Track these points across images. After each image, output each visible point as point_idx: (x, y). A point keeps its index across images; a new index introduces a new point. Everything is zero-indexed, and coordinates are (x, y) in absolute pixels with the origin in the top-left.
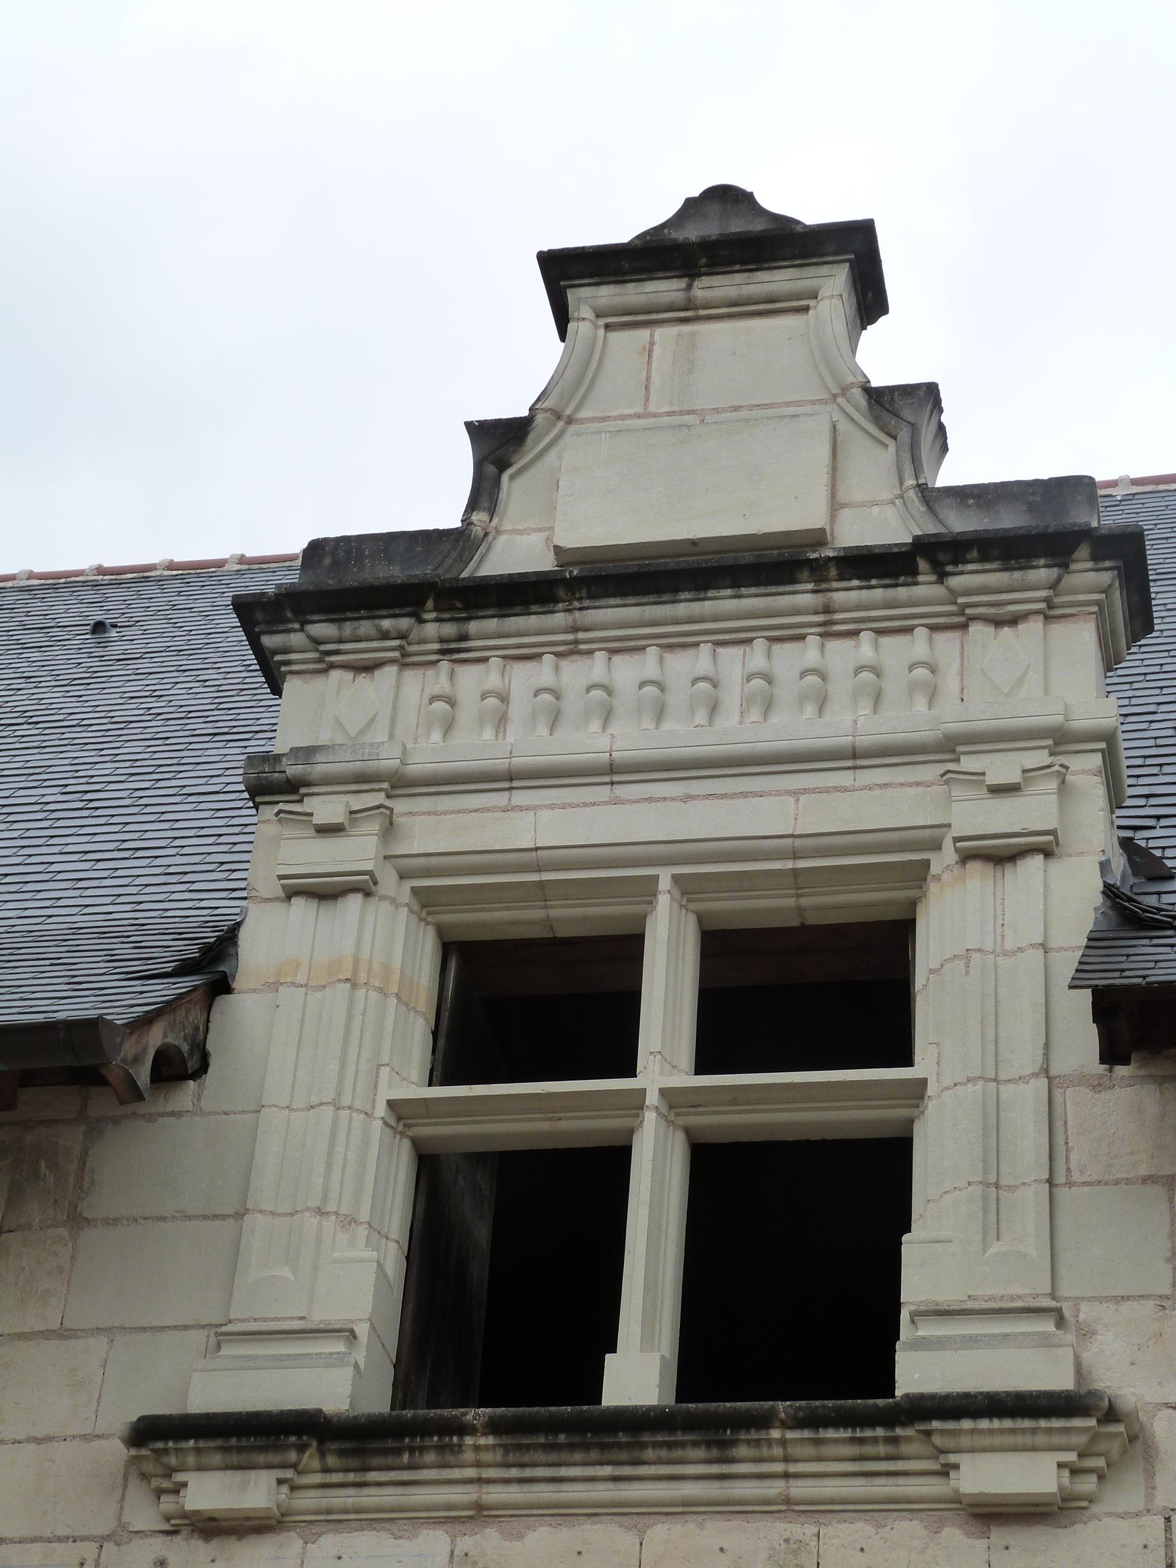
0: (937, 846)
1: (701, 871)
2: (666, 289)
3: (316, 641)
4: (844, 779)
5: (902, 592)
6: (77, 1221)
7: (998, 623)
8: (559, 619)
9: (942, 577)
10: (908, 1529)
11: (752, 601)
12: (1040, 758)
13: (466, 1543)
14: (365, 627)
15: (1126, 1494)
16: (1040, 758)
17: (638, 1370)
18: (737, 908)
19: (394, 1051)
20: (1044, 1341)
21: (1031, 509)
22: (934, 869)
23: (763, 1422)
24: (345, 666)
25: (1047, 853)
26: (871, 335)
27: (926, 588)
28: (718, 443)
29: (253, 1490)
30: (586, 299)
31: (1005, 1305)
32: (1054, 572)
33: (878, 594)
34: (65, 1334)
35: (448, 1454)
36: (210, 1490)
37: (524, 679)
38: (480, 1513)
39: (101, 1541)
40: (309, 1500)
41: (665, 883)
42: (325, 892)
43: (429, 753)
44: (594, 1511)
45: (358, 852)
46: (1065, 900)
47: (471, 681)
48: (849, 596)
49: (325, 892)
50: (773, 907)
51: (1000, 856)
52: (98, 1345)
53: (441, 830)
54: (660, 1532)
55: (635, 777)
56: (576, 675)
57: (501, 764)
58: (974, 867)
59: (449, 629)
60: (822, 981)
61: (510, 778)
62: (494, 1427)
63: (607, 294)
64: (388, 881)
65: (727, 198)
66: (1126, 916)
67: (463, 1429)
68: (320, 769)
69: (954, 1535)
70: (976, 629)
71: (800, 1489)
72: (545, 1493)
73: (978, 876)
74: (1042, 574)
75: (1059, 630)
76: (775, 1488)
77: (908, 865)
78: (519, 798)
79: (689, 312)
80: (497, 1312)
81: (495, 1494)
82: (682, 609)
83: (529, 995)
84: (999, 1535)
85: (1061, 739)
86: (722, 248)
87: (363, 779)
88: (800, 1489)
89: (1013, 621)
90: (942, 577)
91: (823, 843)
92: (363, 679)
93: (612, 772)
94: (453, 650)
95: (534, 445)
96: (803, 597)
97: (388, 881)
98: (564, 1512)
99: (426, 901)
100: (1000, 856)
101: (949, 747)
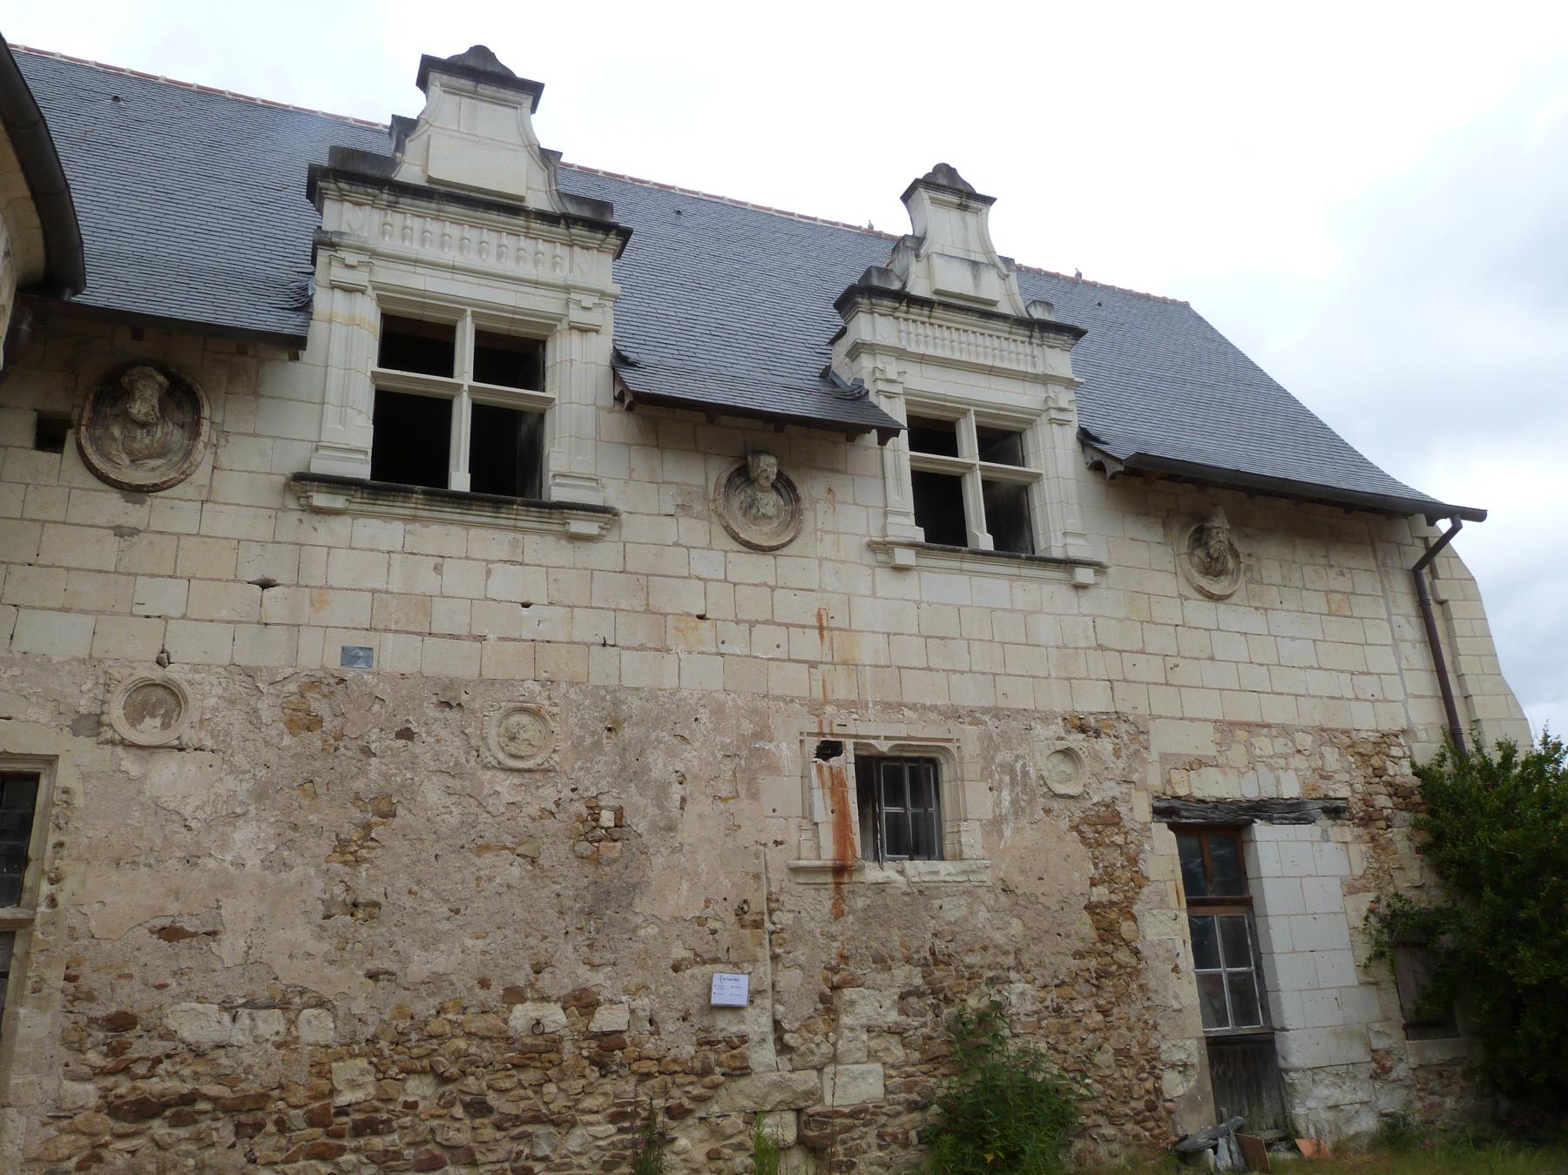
0: (560, 320)
1: (482, 312)
2: (467, 84)
3: (341, 190)
4: (532, 291)
6: (257, 395)
7: (583, 248)
8: (434, 206)
9: (568, 228)
10: (550, 539)
11: (503, 218)
12: (366, 259)
13: (409, 527)
14: (361, 189)
15: (613, 535)
16: (366, 259)
17: (460, 479)
18: (987, 421)
20: (595, 489)
21: (594, 210)
23: (513, 503)
26: (412, 113)
27: (562, 230)
28: (466, 149)
29: (338, 502)
30: (436, 79)
31: (1455, 691)
35: (407, 499)
36: (320, 499)
37: (416, 224)
38: (414, 519)
39: (277, 510)
40: (355, 506)
42: (349, 290)
43: (388, 244)
44: (452, 522)
45: (359, 277)
46: (600, 349)
47: (396, 219)
48: (536, 225)
49: (349, 290)
50: (502, 327)
51: (583, 330)
52: (270, 442)
53: (389, 275)
54: (473, 531)
55: (474, 272)
57: (413, 256)
59: (392, 198)
60: (515, 355)
61: (417, 262)
62: (424, 493)
64: (370, 291)
66: (620, 360)
67: (413, 492)
68: (346, 241)
69: (564, 543)
70: (576, 249)
71: (519, 524)
72: (437, 515)
73: (575, 335)
74: (600, 236)
76: (512, 523)
77: (550, 325)
78: (419, 270)
79: (474, 95)
80: (406, 453)
82: (479, 214)
83: (412, 339)
84: (577, 544)
85: (603, 294)
86: (476, 73)
87: (361, 250)
88: (519, 524)
89: (588, 248)
90: (568, 228)
91: (524, 312)
92: (357, 208)
93: (453, 269)
94: (391, 206)
95: (420, 129)
96: (520, 221)
97: (370, 291)
98: (443, 522)
99: (380, 299)
100: (583, 330)
101: (567, 289)
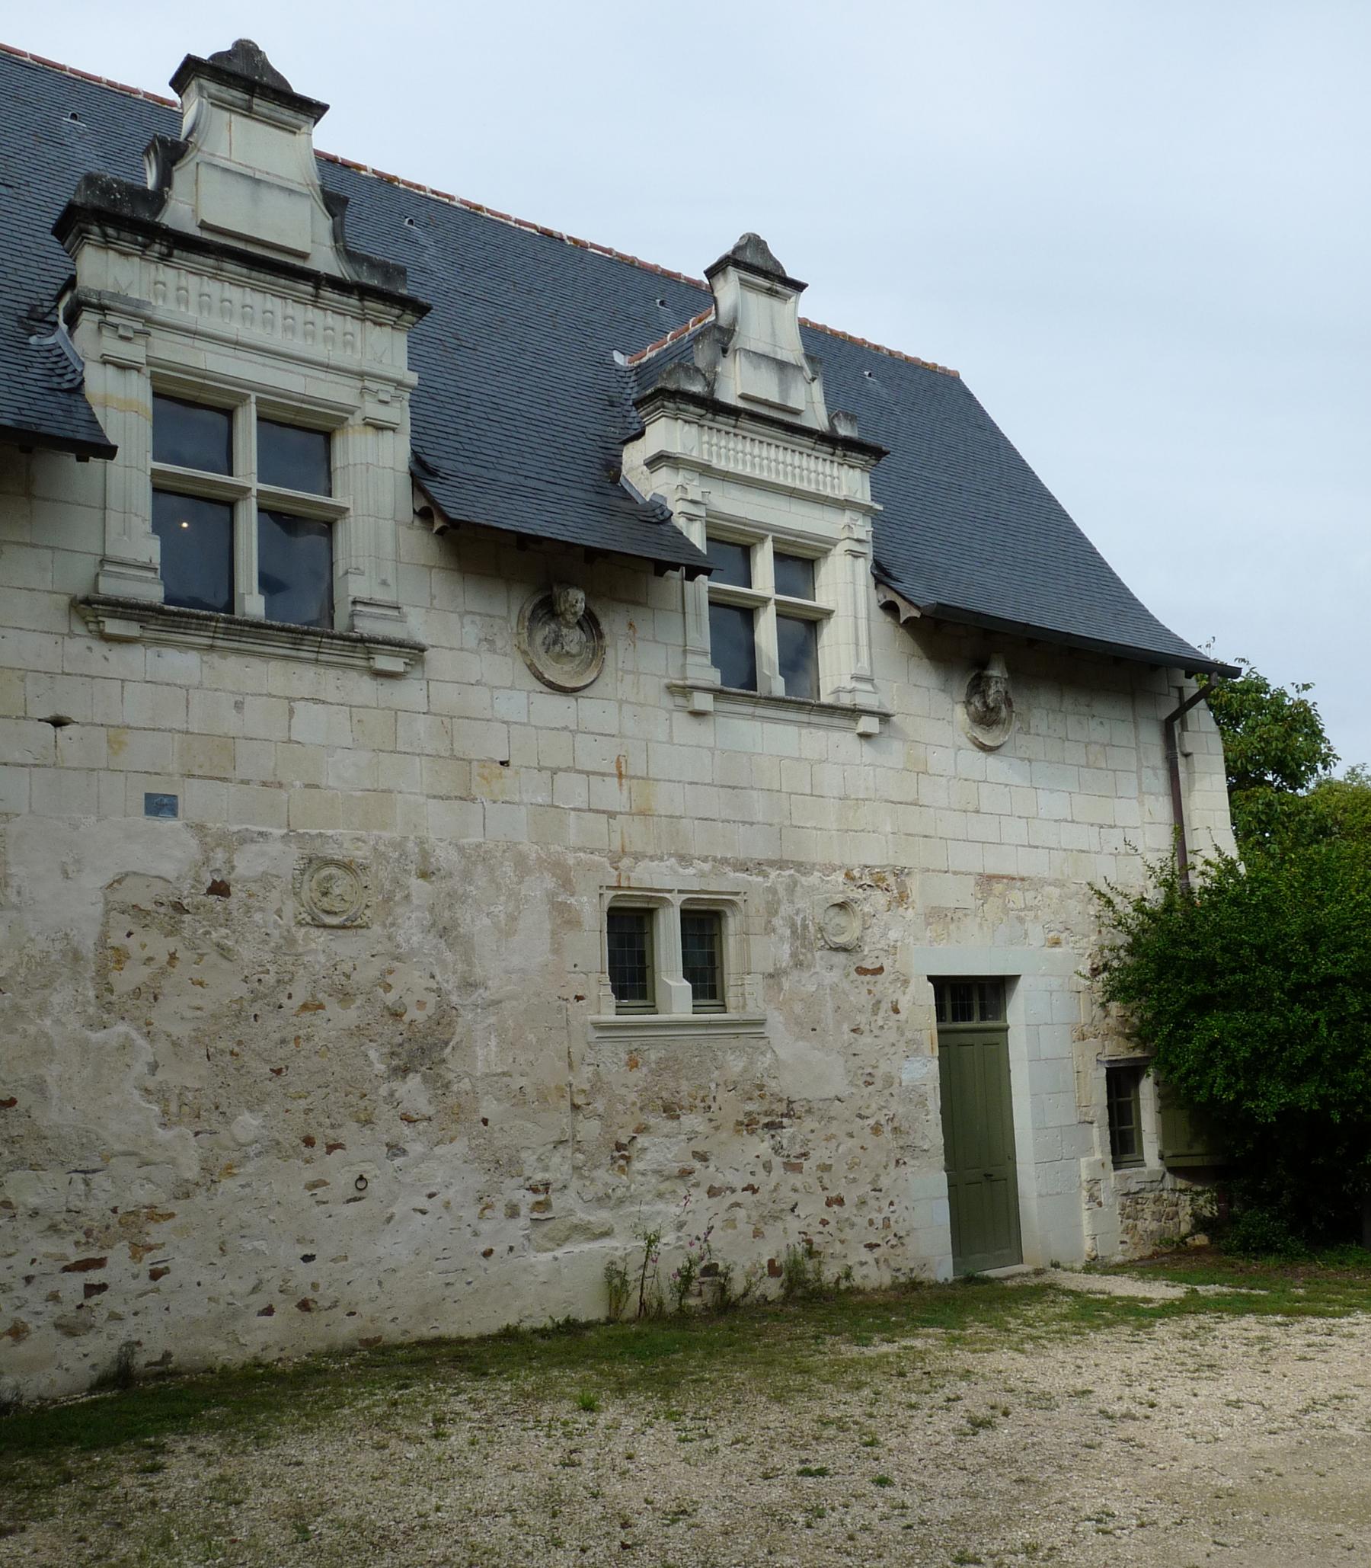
4: (322, 375)
5: (345, 299)
7: (375, 323)
10: (354, 674)
19: (1146, 1157)
22: (351, 422)
24: (116, 250)
25: (393, 430)
32: (415, 319)
33: (336, 297)
34: (34, 546)
40: (148, 634)
41: (253, 399)
45: (133, 352)
49: (123, 367)
56: (212, 287)
57: (193, 327)
58: (369, 429)
63: (213, 87)
65: (246, 50)
69: (366, 678)
72: (236, 645)
75: (396, 334)
78: (197, 343)
81: (219, 643)
84: (380, 680)
89: (381, 325)
90: (361, 300)
101: (361, 375)
